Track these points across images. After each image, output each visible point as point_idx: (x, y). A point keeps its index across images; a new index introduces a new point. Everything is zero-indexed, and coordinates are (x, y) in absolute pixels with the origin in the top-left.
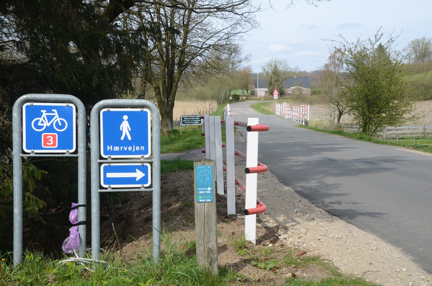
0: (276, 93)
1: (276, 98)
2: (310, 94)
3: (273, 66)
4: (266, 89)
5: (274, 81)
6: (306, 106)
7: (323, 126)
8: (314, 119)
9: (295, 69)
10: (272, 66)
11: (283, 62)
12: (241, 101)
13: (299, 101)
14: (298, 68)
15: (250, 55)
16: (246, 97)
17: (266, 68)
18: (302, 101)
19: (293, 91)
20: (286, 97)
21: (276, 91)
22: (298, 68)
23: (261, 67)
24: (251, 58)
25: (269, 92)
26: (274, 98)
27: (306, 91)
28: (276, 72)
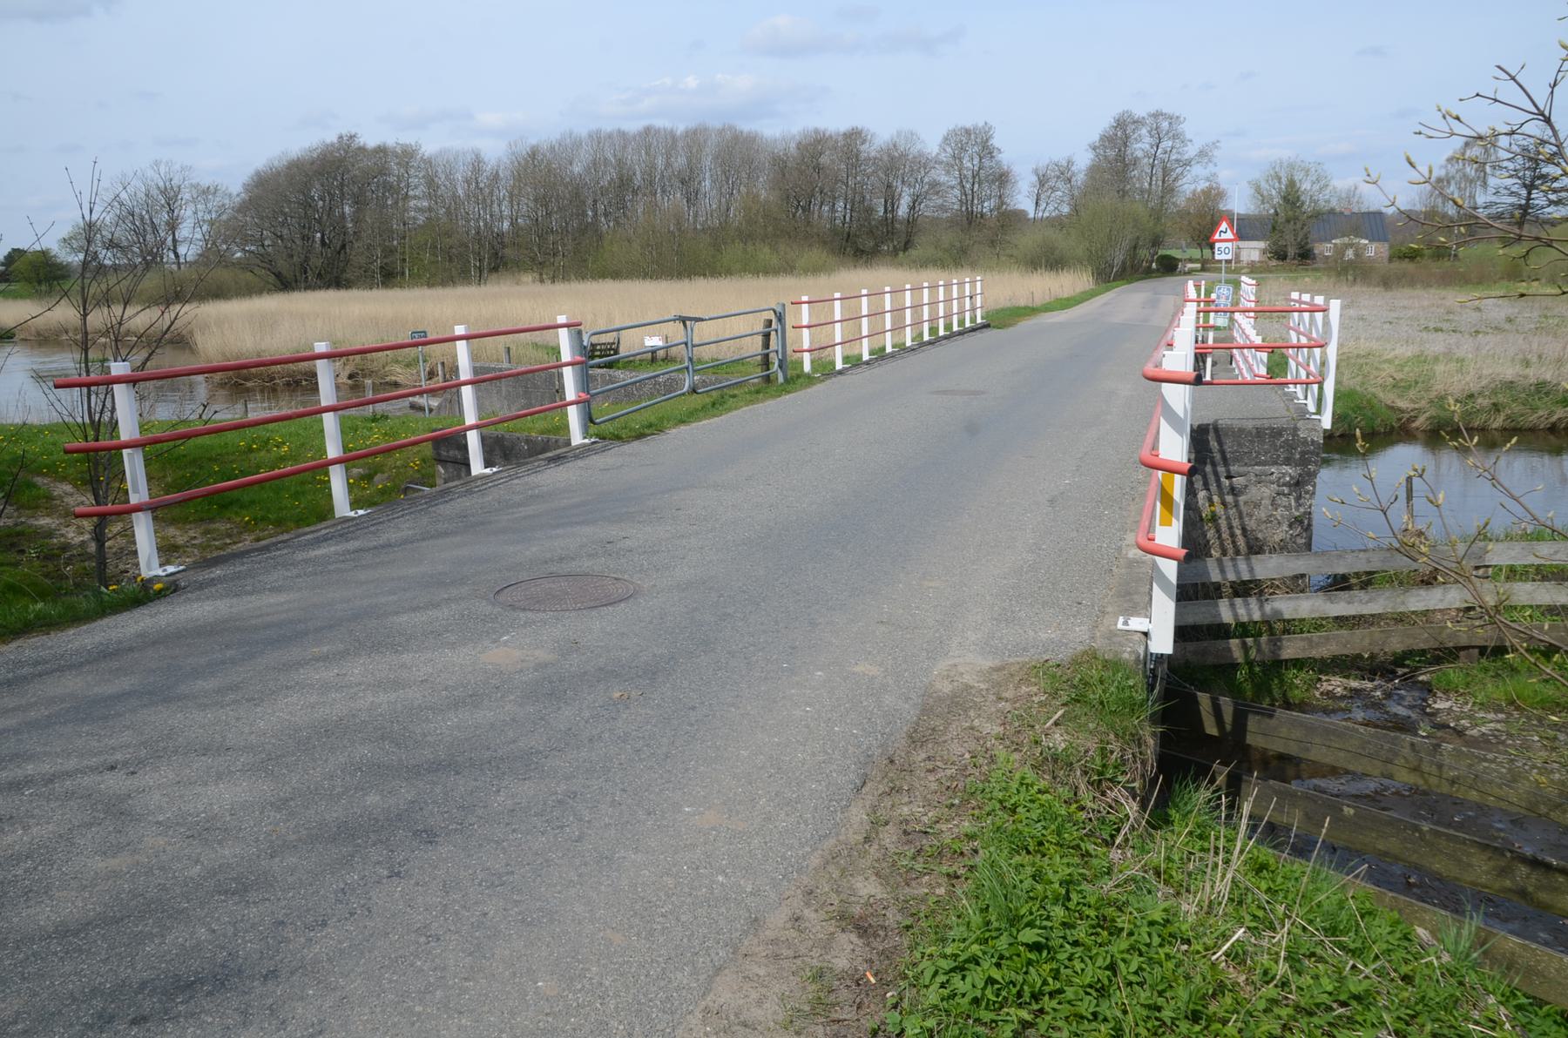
0: (1224, 236)
1: (1223, 257)
2: (1386, 261)
3: (1284, 180)
4: (1262, 245)
5: (1283, 220)
6: (1319, 300)
7: (1433, 394)
8: (1389, 346)
9: (1349, 190)
10: (1279, 179)
11: (1313, 169)
12: (1178, 275)
13: (1349, 277)
14: (1356, 188)
15: (1215, 144)
16: (1203, 265)
17: (1264, 185)
18: (1359, 280)
19: (1340, 251)
20: (1316, 266)
21: (1224, 226)
22: (1356, 188)
23: (1249, 182)
24: (1216, 153)
25: (1270, 253)
26: (1217, 257)
27: (1373, 250)
28: (1291, 198)
